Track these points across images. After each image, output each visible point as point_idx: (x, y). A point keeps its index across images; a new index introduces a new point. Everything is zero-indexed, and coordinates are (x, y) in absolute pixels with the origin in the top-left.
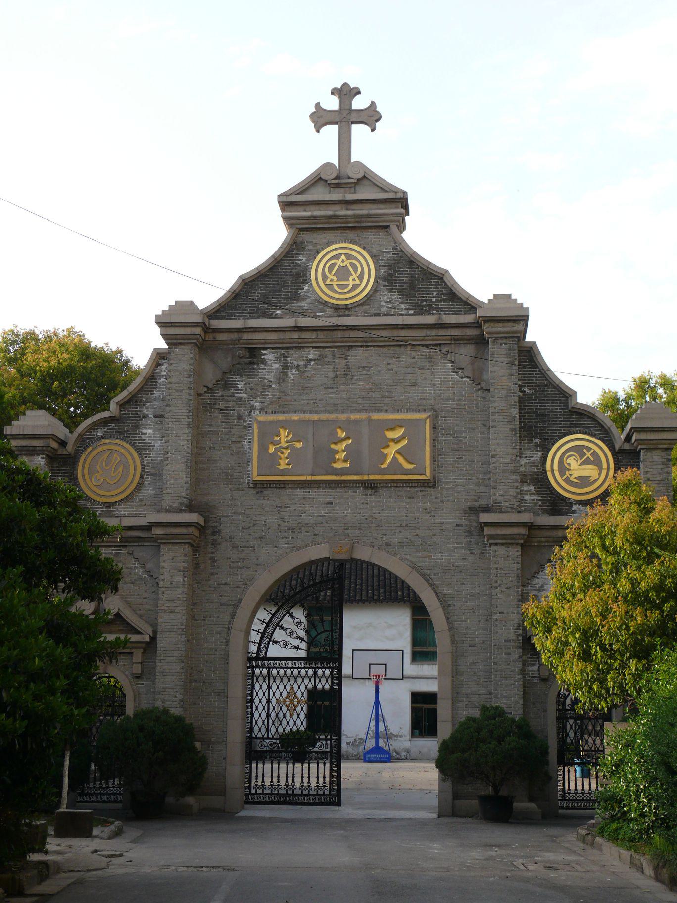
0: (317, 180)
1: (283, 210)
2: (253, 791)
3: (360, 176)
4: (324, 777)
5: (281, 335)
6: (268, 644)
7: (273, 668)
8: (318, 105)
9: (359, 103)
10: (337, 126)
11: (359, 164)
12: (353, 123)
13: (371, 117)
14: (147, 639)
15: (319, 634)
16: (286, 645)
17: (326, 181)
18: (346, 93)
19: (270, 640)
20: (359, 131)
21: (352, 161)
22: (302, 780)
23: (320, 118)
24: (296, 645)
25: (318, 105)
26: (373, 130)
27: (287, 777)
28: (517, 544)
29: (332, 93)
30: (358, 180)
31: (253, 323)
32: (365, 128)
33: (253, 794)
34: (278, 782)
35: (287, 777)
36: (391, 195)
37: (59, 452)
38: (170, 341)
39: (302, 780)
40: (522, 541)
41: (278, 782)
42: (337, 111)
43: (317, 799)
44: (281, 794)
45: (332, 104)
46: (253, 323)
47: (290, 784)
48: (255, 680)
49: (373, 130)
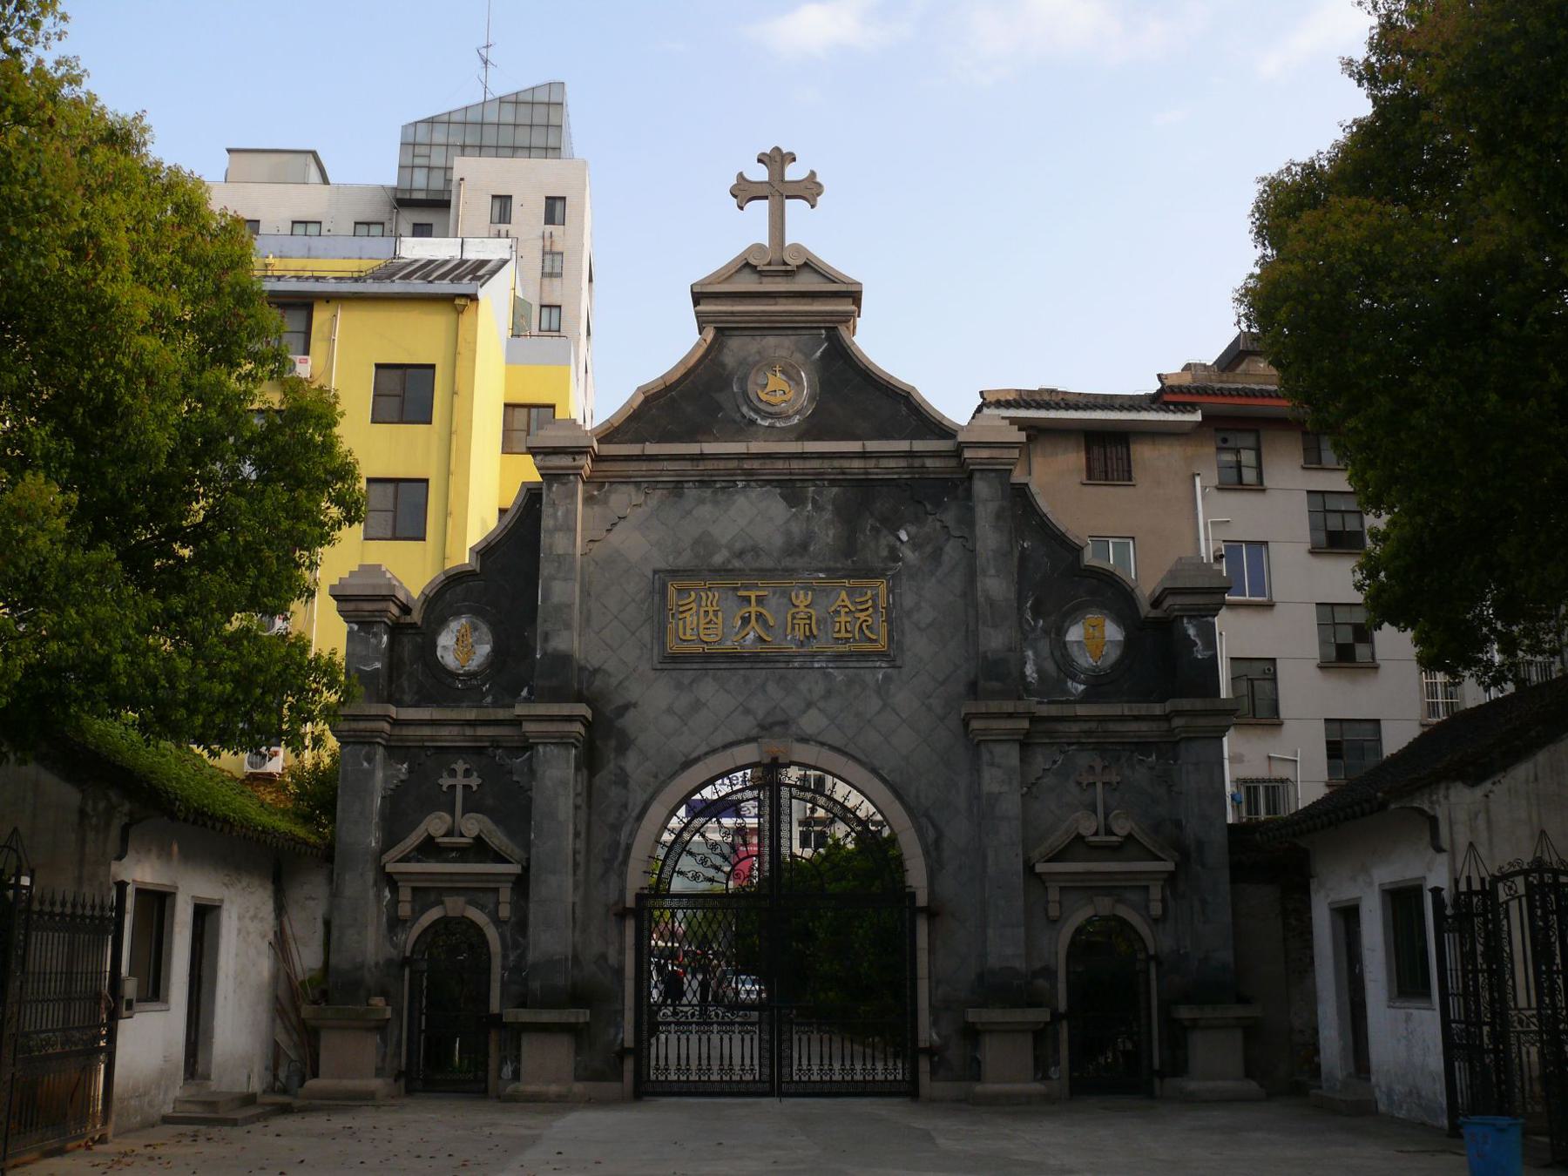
0: (745, 266)
1: (696, 302)
2: (796, 1078)
3: (800, 262)
4: (752, 1058)
5: (996, 453)
6: (671, 876)
7: (678, 909)
8: (741, 175)
9: (793, 173)
10: (766, 203)
11: (798, 248)
12: (788, 197)
13: (809, 190)
14: (515, 869)
15: (741, 860)
16: (695, 877)
17: (756, 267)
18: (776, 159)
19: (674, 871)
20: (794, 208)
21: (787, 243)
22: (743, 1061)
23: (744, 192)
24: (710, 876)
25: (741, 175)
26: (813, 207)
27: (700, 1058)
28: (1014, 741)
29: (760, 161)
30: (798, 267)
31: (709, 448)
32: (801, 204)
33: (796, 1082)
34: (688, 1064)
35: (700, 1058)
36: (843, 288)
37: (402, 621)
38: (543, 472)
39: (743, 1061)
40: (1022, 738)
41: (688, 1064)
42: (766, 182)
43: (743, 1087)
44: (835, 1082)
45: (760, 174)
46: (709, 448)
47: (662, 1067)
48: (653, 925)
49: (813, 207)
